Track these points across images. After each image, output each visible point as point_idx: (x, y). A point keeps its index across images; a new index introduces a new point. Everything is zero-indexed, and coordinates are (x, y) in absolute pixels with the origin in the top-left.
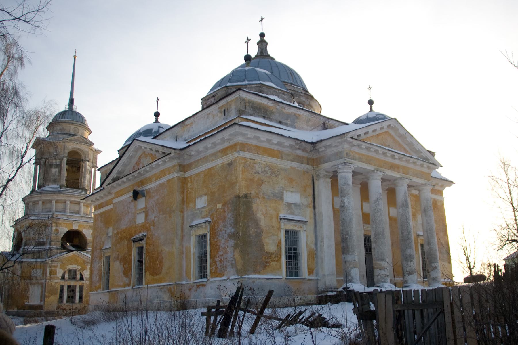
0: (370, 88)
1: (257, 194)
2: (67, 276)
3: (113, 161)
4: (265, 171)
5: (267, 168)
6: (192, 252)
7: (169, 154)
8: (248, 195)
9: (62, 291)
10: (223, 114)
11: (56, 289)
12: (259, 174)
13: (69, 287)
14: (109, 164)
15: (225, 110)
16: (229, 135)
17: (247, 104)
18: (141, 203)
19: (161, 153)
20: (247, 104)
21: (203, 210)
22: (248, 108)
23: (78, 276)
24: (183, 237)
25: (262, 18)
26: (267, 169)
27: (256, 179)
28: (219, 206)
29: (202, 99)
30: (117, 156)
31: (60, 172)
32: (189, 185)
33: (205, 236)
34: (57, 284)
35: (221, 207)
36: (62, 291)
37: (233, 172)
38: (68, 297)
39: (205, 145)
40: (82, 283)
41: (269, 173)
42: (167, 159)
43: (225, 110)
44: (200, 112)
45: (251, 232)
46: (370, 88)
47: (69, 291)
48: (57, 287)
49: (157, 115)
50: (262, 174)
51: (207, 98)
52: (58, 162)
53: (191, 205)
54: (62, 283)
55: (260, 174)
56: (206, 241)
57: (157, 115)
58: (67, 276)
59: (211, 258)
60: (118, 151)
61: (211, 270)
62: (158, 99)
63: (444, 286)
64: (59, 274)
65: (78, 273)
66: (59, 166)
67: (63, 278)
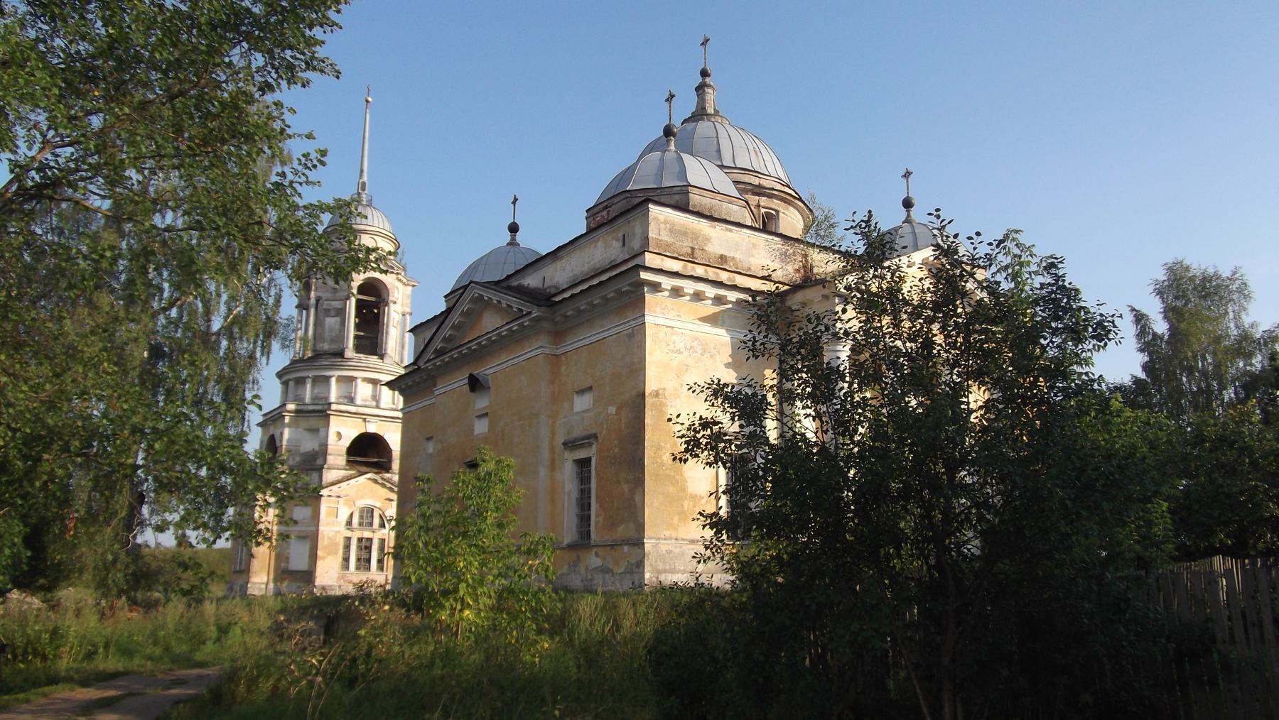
0: (907, 175)
1: (676, 390)
2: (356, 520)
3: (435, 317)
4: (692, 347)
5: (696, 342)
6: (566, 490)
7: (529, 313)
8: (661, 392)
9: (347, 547)
10: (621, 244)
11: (337, 544)
12: (680, 352)
13: (360, 540)
14: (428, 321)
15: (624, 236)
16: (629, 285)
17: (662, 226)
18: (482, 402)
19: (515, 310)
20: (662, 226)
21: (586, 415)
22: (663, 233)
23: (376, 521)
24: (553, 462)
25: (670, 95)
26: (695, 344)
27: (675, 363)
28: (612, 410)
29: (587, 211)
30: (442, 307)
31: (343, 323)
32: (563, 368)
33: (588, 461)
34: (338, 534)
35: (614, 413)
36: (347, 547)
37: (635, 350)
38: (359, 560)
39: (589, 300)
40: (383, 534)
41: (699, 351)
42: (525, 322)
43: (624, 236)
44: (582, 236)
45: (664, 458)
46: (907, 175)
47: (360, 548)
48: (338, 540)
49: (514, 228)
50: (686, 353)
51: (596, 210)
52: (337, 304)
53: (566, 405)
54: (349, 534)
55: (682, 353)
56: (590, 471)
57: (514, 228)
58: (356, 520)
59: (597, 501)
60: (445, 297)
61: (597, 523)
62: (516, 200)
63: (119, 693)
64: (344, 517)
65: (376, 514)
66: (341, 312)
67: (349, 523)
